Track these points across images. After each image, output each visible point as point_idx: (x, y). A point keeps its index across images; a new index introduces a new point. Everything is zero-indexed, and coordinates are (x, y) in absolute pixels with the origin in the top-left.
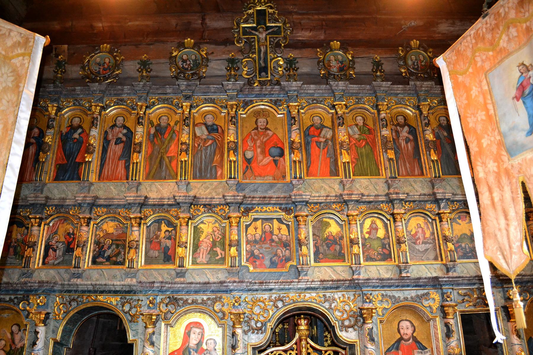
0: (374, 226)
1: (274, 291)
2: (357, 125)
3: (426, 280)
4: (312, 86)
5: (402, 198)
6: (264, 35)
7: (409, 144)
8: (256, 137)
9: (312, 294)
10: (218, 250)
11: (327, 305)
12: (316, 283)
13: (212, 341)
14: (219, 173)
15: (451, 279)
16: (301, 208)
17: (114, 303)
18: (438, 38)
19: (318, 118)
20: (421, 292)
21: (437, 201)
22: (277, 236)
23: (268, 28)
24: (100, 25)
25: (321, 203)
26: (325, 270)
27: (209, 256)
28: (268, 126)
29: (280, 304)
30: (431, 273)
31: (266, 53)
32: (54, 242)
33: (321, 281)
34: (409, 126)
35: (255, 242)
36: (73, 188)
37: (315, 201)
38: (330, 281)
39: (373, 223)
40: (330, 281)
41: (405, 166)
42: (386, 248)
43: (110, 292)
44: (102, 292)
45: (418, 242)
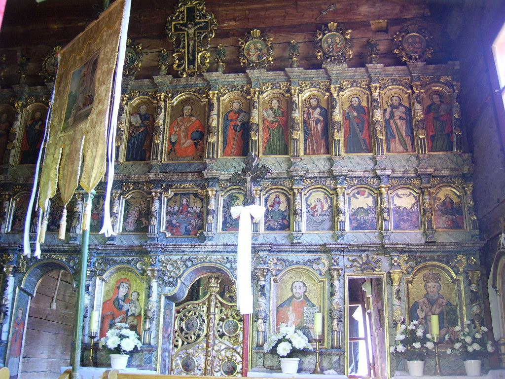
0: (277, 200)
1: (186, 253)
2: (272, 108)
3: (317, 247)
4: (231, 74)
5: (301, 174)
6: (193, 31)
7: (319, 125)
8: (181, 123)
9: (218, 256)
10: (144, 220)
11: (228, 265)
12: (220, 247)
13: (136, 293)
14: (148, 155)
15: (337, 246)
16: (213, 184)
17: (64, 259)
18: (360, 20)
19: (237, 103)
20: (314, 257)
21: (335, 178)
22: (192, 208)
23: (196, 24)
24: (56, 27)
25: (316, 178)
26: (229, 236)
27: (136, 225)
28: (192, 113)
29: (189, 264)
30: (323, 241)
31: (194, 47)
32: (19, 213)
33: (224, 245)
34: (321, 108)
35: (174, 213)
36: (18, 129)
37: (225, 178)
38: (232, 245)
39: (277, 197)
40: (232, 245)
41: (312, 145)
42: (286, 219)
43: (60, 251)
44: (55, 252)
45: (316, 214)
